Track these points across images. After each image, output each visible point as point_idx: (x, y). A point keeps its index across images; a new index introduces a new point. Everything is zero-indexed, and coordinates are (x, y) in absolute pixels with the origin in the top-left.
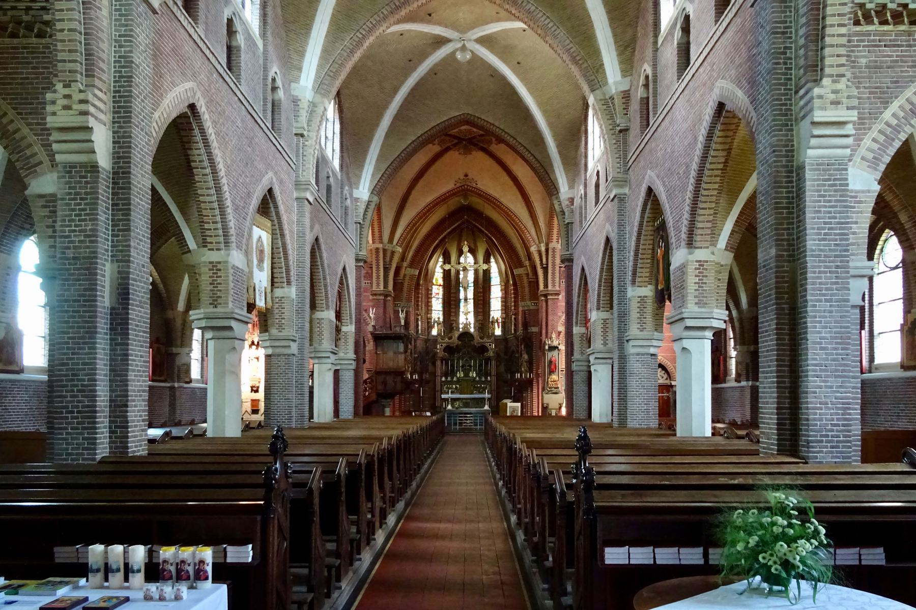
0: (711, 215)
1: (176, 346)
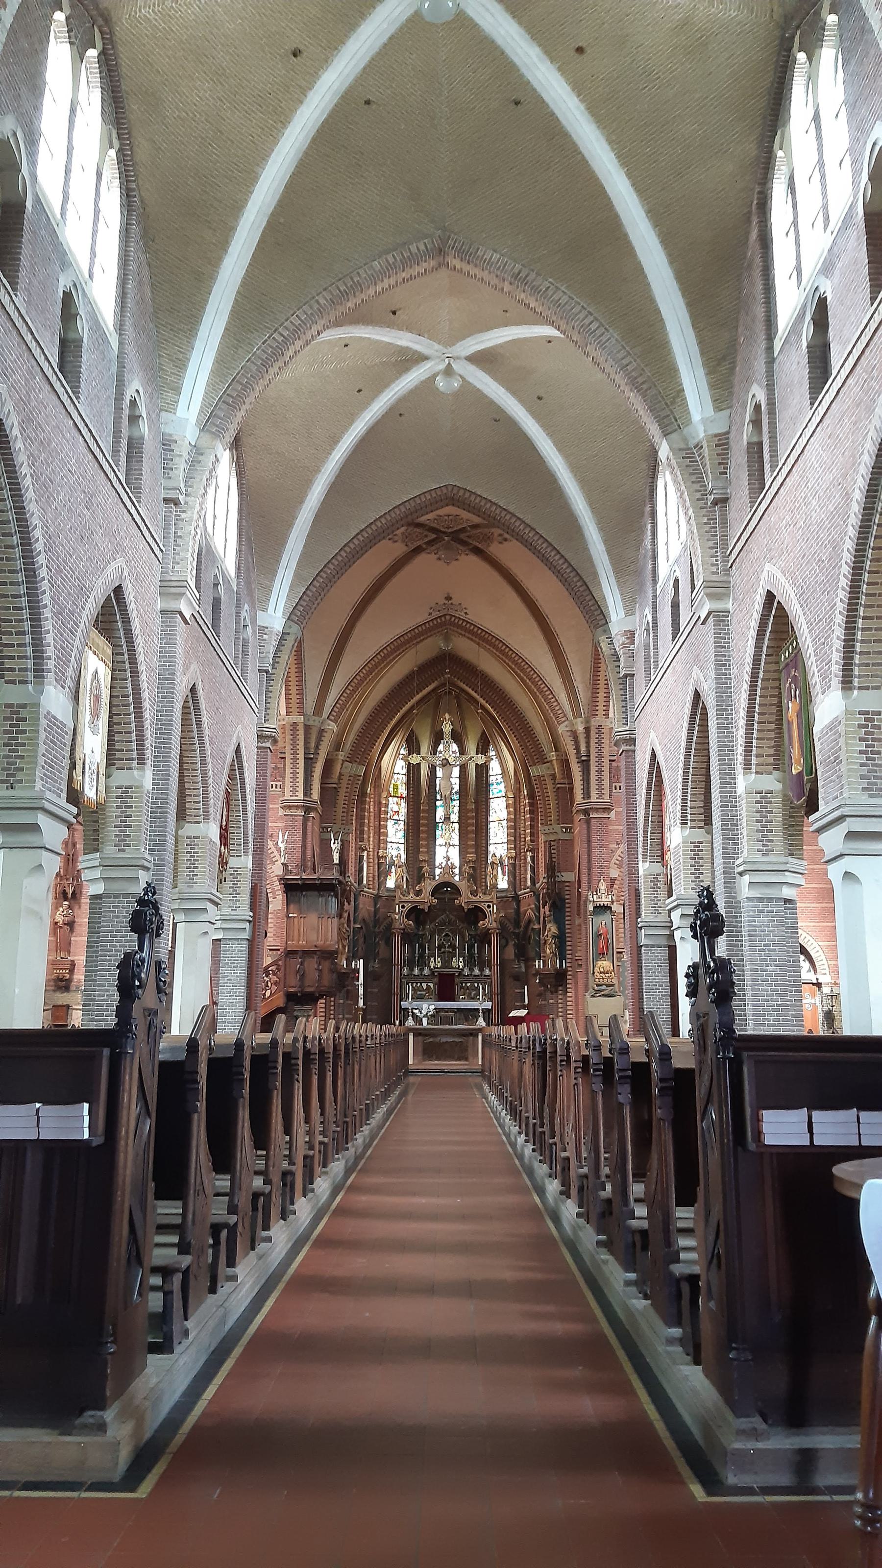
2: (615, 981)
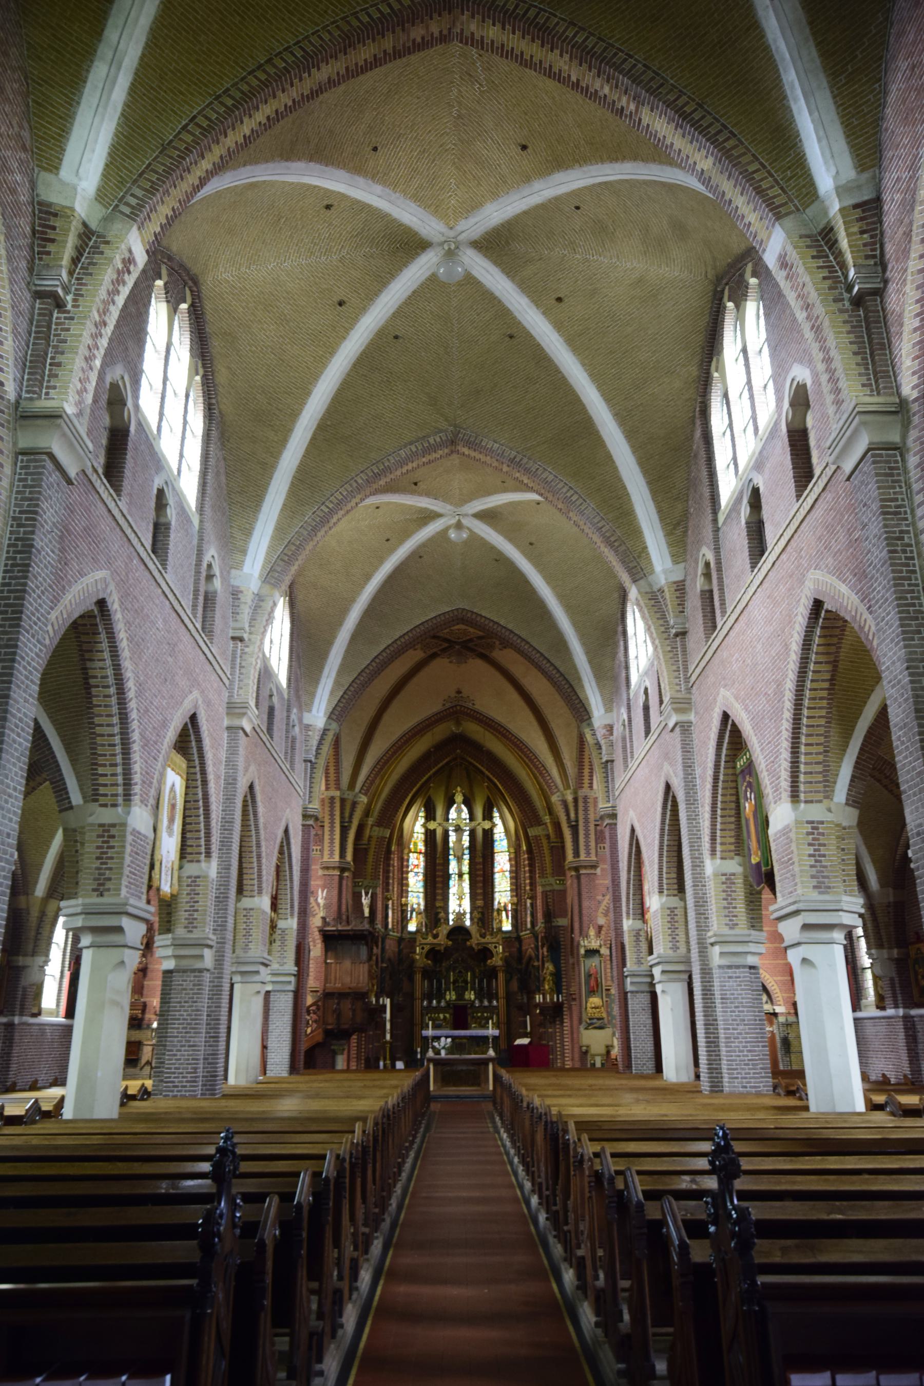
0: (820, 753)
1: (25, 955)
2: (604, 1015)
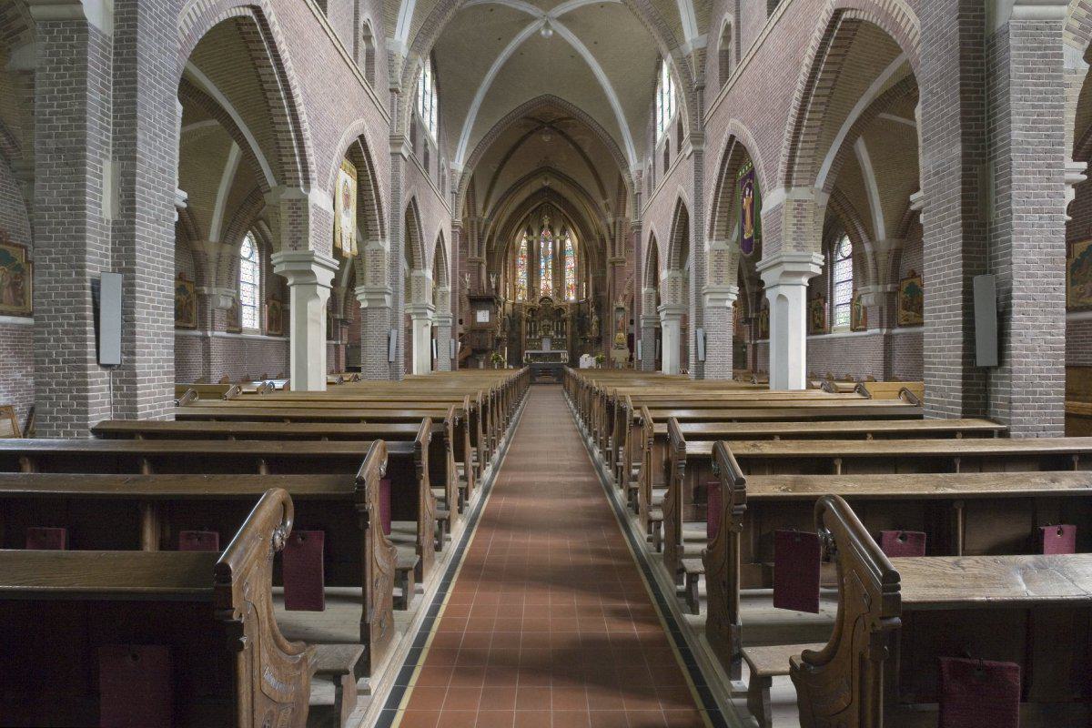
0: (812, 149)
